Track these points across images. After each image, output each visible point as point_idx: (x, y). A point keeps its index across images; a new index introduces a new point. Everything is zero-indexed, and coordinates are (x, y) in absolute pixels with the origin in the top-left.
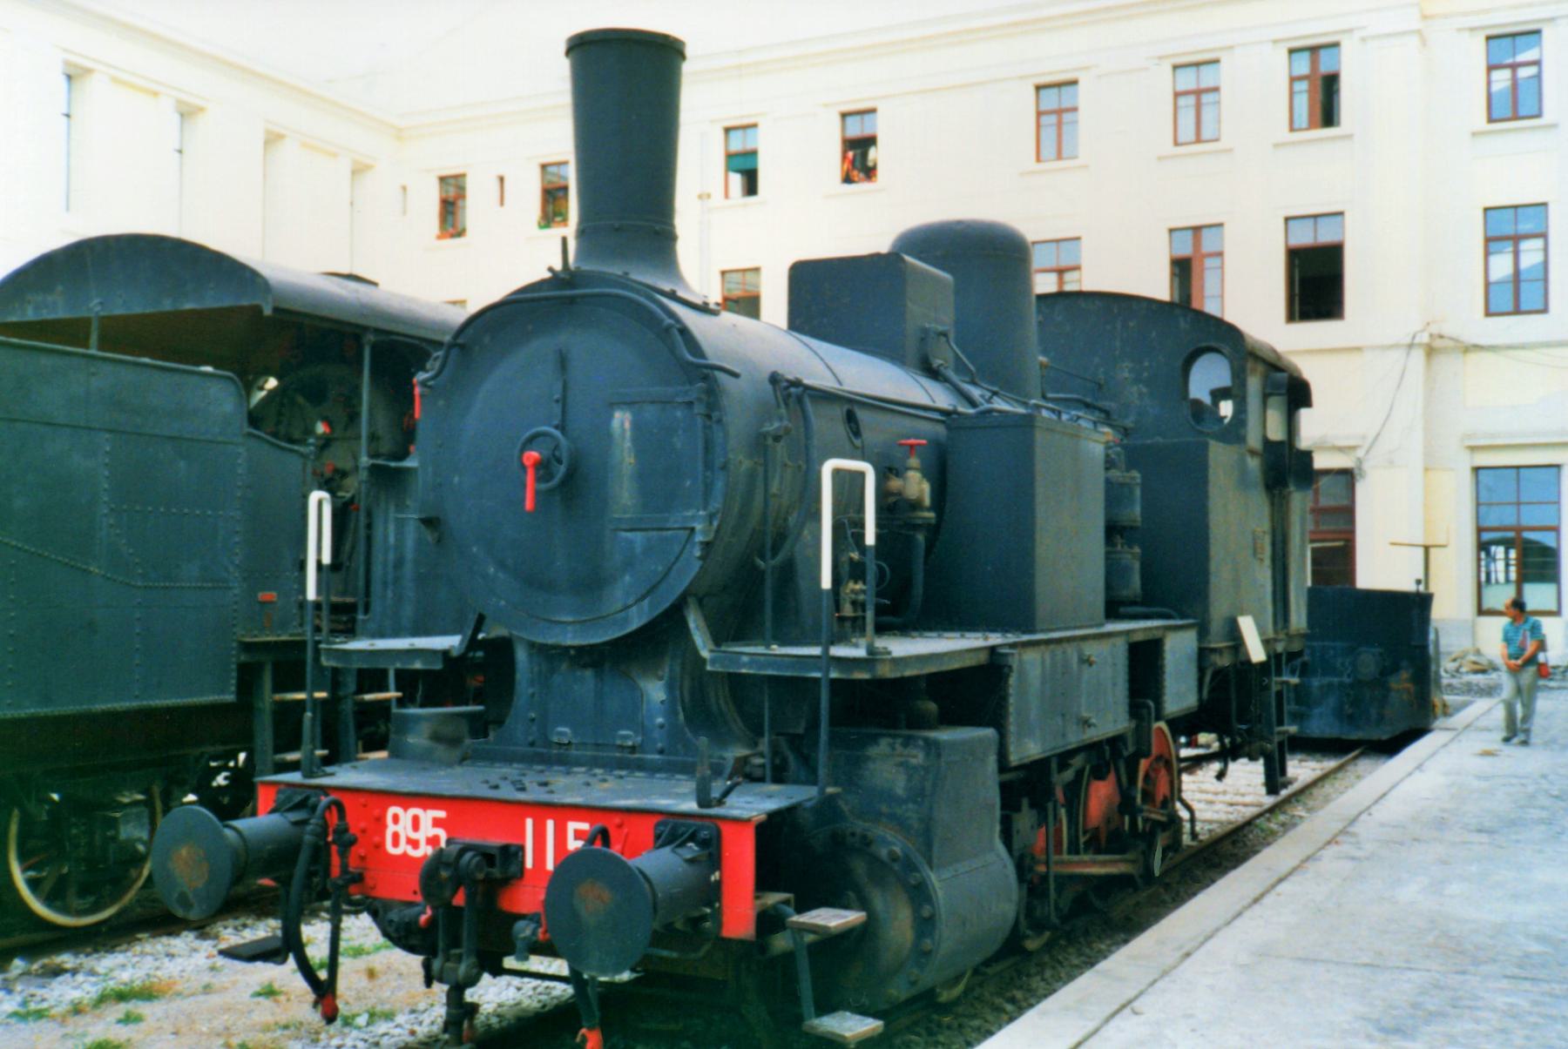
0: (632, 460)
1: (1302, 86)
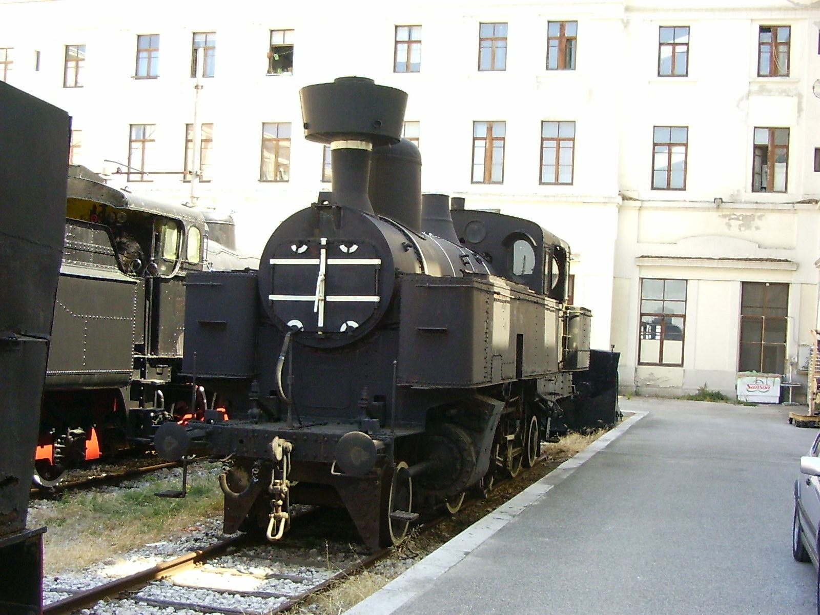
0: (262, 571)
1: (556, 42)
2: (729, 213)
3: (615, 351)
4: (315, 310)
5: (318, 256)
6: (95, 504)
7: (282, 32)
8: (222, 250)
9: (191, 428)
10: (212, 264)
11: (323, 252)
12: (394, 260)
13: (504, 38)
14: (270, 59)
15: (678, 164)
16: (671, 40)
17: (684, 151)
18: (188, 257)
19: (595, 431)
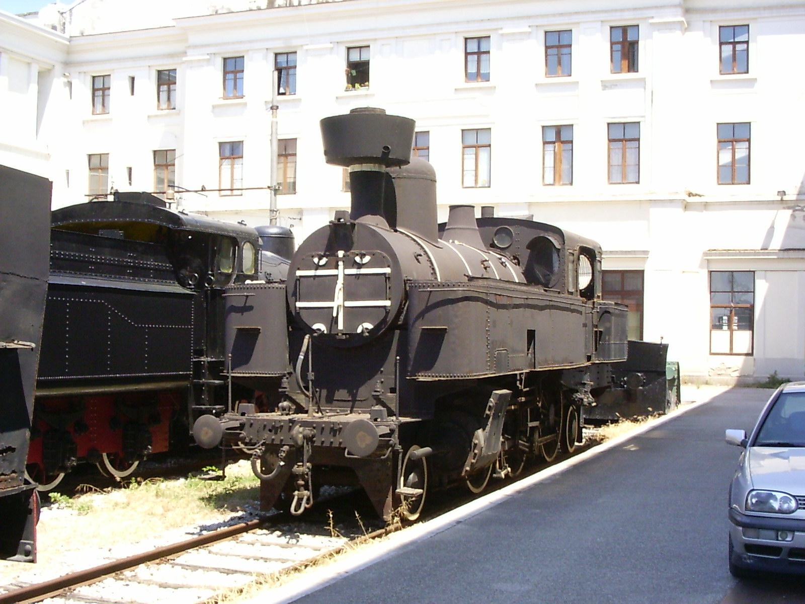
1: (619, 47)
2: (793, 205)
3: (664, 342)
4: (335, 315)
5: (337, 267)
6: (158, 490)
7: (358, 49)
8: (282, 261)
9: (228, 420)
10: (270, 274)
11: (341, 263)
12: (401, 268)
13: (569, 45)
14: (348, 75)
15: (741, 159)
16: (730, 39)
17: (747, 146)
18: (244, 270)
19: (645, 418)
